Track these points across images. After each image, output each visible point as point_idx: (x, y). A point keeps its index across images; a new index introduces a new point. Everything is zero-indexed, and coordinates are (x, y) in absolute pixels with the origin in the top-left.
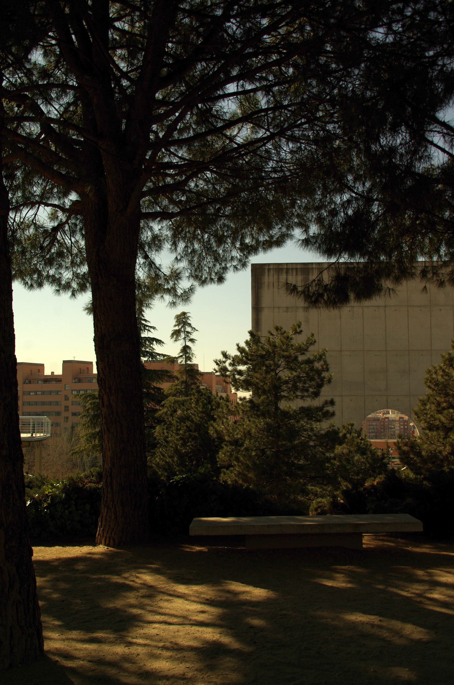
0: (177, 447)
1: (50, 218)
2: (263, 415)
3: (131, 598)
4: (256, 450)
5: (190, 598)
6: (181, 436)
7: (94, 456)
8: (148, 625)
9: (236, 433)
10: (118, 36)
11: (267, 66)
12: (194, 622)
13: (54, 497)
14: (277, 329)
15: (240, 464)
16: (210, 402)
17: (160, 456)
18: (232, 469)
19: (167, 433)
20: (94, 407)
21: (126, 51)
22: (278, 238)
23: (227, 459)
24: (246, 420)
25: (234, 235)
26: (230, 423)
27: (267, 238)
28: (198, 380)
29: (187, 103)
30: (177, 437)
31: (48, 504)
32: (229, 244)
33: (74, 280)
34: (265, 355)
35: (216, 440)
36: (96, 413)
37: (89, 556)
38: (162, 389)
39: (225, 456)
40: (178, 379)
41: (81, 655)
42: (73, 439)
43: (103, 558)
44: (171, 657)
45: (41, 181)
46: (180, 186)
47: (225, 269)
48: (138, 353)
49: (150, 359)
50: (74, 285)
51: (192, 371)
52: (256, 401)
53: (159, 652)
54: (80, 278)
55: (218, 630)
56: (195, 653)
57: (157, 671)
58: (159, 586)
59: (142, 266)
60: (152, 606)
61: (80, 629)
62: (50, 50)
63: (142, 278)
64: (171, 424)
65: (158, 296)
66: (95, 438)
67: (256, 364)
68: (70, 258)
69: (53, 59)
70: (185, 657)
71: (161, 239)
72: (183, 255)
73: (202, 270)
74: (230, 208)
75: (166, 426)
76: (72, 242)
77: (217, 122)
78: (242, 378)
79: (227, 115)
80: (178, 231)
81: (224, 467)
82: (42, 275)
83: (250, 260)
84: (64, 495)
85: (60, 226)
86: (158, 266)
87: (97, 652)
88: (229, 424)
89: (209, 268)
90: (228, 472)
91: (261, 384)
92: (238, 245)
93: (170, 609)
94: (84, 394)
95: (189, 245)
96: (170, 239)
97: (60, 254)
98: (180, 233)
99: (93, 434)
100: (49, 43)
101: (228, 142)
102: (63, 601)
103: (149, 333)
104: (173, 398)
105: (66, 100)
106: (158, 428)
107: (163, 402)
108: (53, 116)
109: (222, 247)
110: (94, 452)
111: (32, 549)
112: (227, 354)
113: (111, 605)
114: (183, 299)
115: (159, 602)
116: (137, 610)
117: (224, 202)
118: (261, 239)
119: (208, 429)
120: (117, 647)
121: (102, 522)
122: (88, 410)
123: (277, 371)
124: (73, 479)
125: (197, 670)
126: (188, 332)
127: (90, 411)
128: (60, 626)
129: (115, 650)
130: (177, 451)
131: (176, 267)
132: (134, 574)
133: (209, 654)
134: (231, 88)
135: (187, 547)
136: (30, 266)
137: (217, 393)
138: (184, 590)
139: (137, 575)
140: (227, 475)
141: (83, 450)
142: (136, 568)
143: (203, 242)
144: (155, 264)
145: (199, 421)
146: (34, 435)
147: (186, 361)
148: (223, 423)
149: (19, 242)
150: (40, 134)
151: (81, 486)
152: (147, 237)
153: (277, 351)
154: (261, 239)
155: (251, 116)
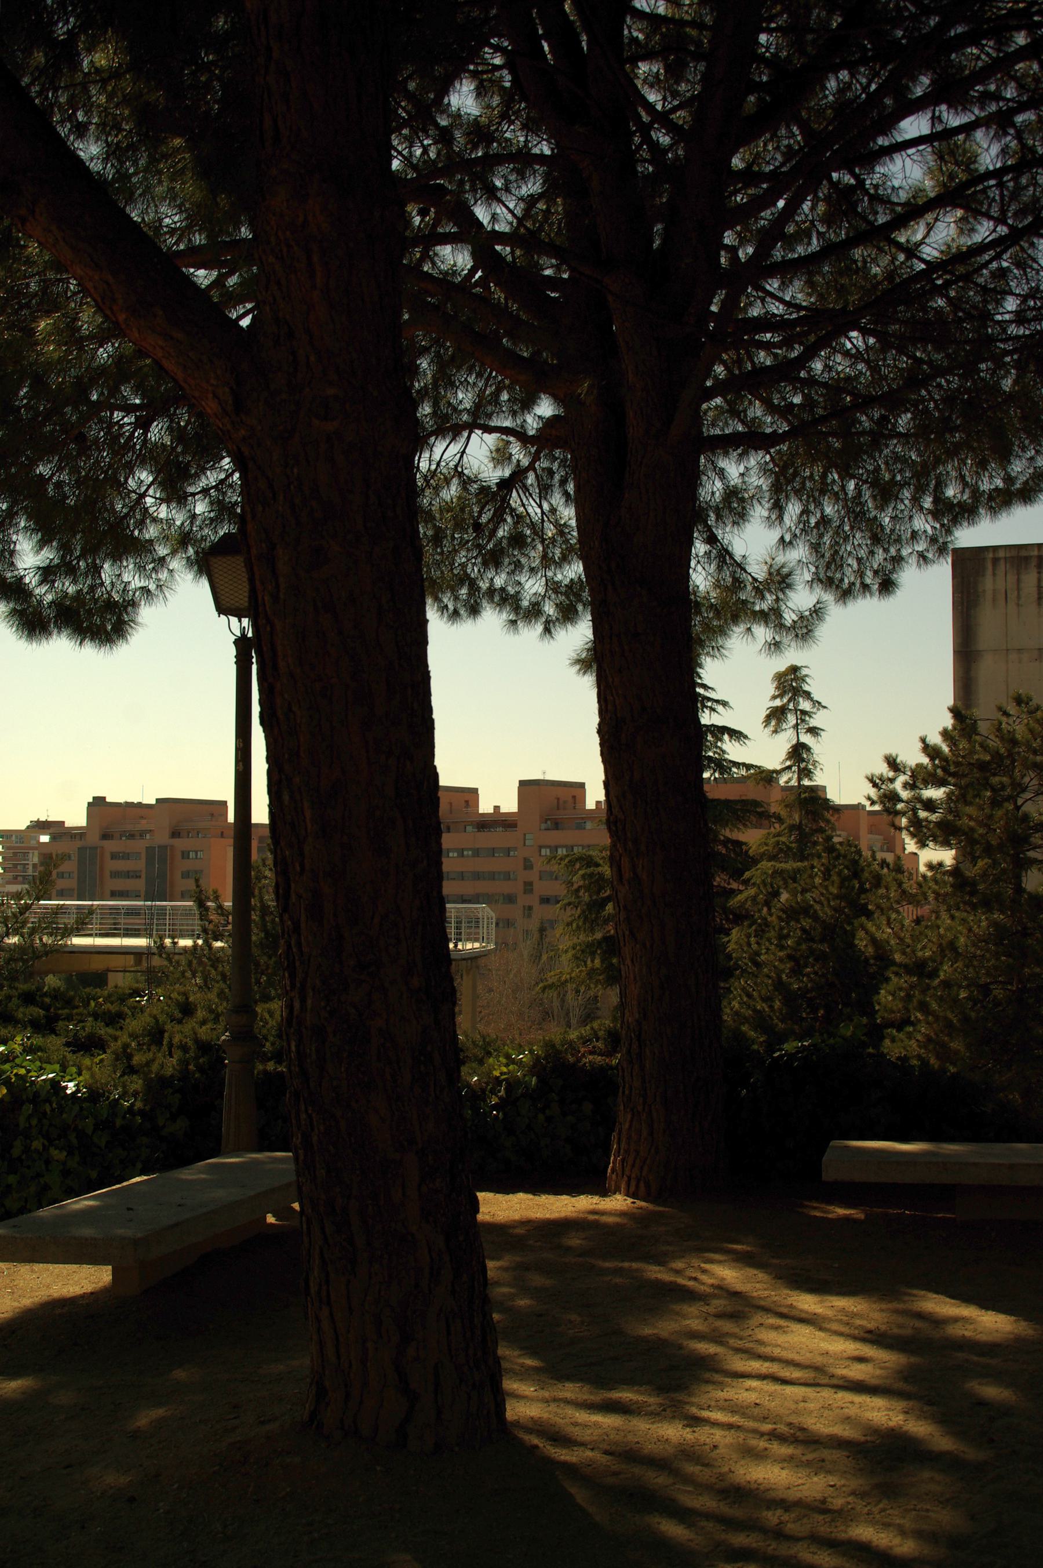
0: (780, 978)
1: (493, 459)
2: (987, 904)
3: (693, 1318)
4: (968, 986)
5: (828, 1326)
6: (789, 951)
7: (591, 993)
8: (735, 1382)
9: (919, 946)
10: (640, 31)
11: (1002, 66)
12: (841, 1382)
13: (512, 1084)
14: (1019, 701)
15: (930, 1018)
16: (856, 874)
17: (740, 996)
18: (911, 1029)
19: (758, 943)
20: (590, 884)
21: (661, 66)
22: (1026, 483)
23: (900, 1006)
24: (944, 915)
25: (918, 480)
26: (907, 922)
27: (999, 483)
28: (828, 821)
29: (803, 174)
30: (781, 954)
31: (500, 1098)
32: (906, 502)
33: (549, 598)
34: (988, 762)
35: (872, 961)
36: (594, 897)
37: (591, 1217)
38: (745, 844)
39: (893, 1000)
40: (780, 819)
41: (587, 1438)
42: (544, 957)
43: (625, 1224)
44: (791, 1458)
45: (474, 376)
46: (787, 372)
47: (898, 560)
48: (699, 763)
49: (717, 775)
50: (549, 609)
51: (813, 803)
52: (971, 872)
53: (762, 1444)
54: (561, 593)
55: (901, 1405)
56: (847, 1454)
57: (761, 1487)
58: (755, 1294)
59: (702, 560)
60: (741, 1339)
61: (581, 1380)
62: (490, 80)
63: (701, 588)
64: (767, 924)
65: (738, 630)
66: (593, 954)
67: (967, 786)
68: (540, 547)
69: (496, 101)
70: (823, 1460)
71: (746, 496)
72: (798, 532)
73: (842, 566)
74: (909, 415)
75: (754, 927)
76: (543, 513)
77: (876, 213)
78: (934, 817)
79: (901, 193)
80: (785, 477)
81: (892, 1025)
82: (479, 589)
83: (956, 539)
84: (534, 1079)
85: (514, 480)
86: (738, 559)
87: (622, 1434)
88: (903, 926)
89: (859, 560)
90: (901, 1035)
91: (981, 831)
92: (928, 502)
93: (784, 1348)
94: (567, 856)
95: (812, 507)
96: (767, 495)
97: (517, 540)
98: (789, 482)
99: (589, 945)
100: (489, 64)
101: (902, 257)
102: (541, 1315)
103: (714, 715)
104: (770, 864)
105: (532, 186)
106: (735, 933)
107: (747, 873)
108: (502, 227)
109: (890, 510)
110: (592, 986)
111: (477, 1197)
112: (898, 760)
113: (647, 1331)
114: (797, 636)
115: (757, 1330)
116: (706, 1346)
117: (894, 402)
118: (985, 486)
119: (854, 936)
120: (665, 1426)
121: (619, 1144)
122: (577, 890)
123: (1020, 802)
124: (553, 1046)
125: (853, 1493)
126: (804, 712)
127: (581, 894)
128: (537, 1370)
129: (661, 1432)
130: (779, 985)
131: (780, 559)
132: (695, 1262)
133: (882, 1459)
134: (914, 126)
135: (815, 1208)
136: (452, 569)
137: (874, 852)
138: (813, 1307)
139: (703, 1265)
140: (899, 1044)
141: (566, 981)
142: (700, 1250)
143: (846, 500)
144: (731, 556)
145: (832, 917)
146: (460, 947)
147: (799, 779)
148: (889, 924)
149: (429, 517)
150: (472, 271)
151: (571, 1060)
152: (713, 493)
153: (1019, 753)
154: (985, 486)
155: (959, 193)
